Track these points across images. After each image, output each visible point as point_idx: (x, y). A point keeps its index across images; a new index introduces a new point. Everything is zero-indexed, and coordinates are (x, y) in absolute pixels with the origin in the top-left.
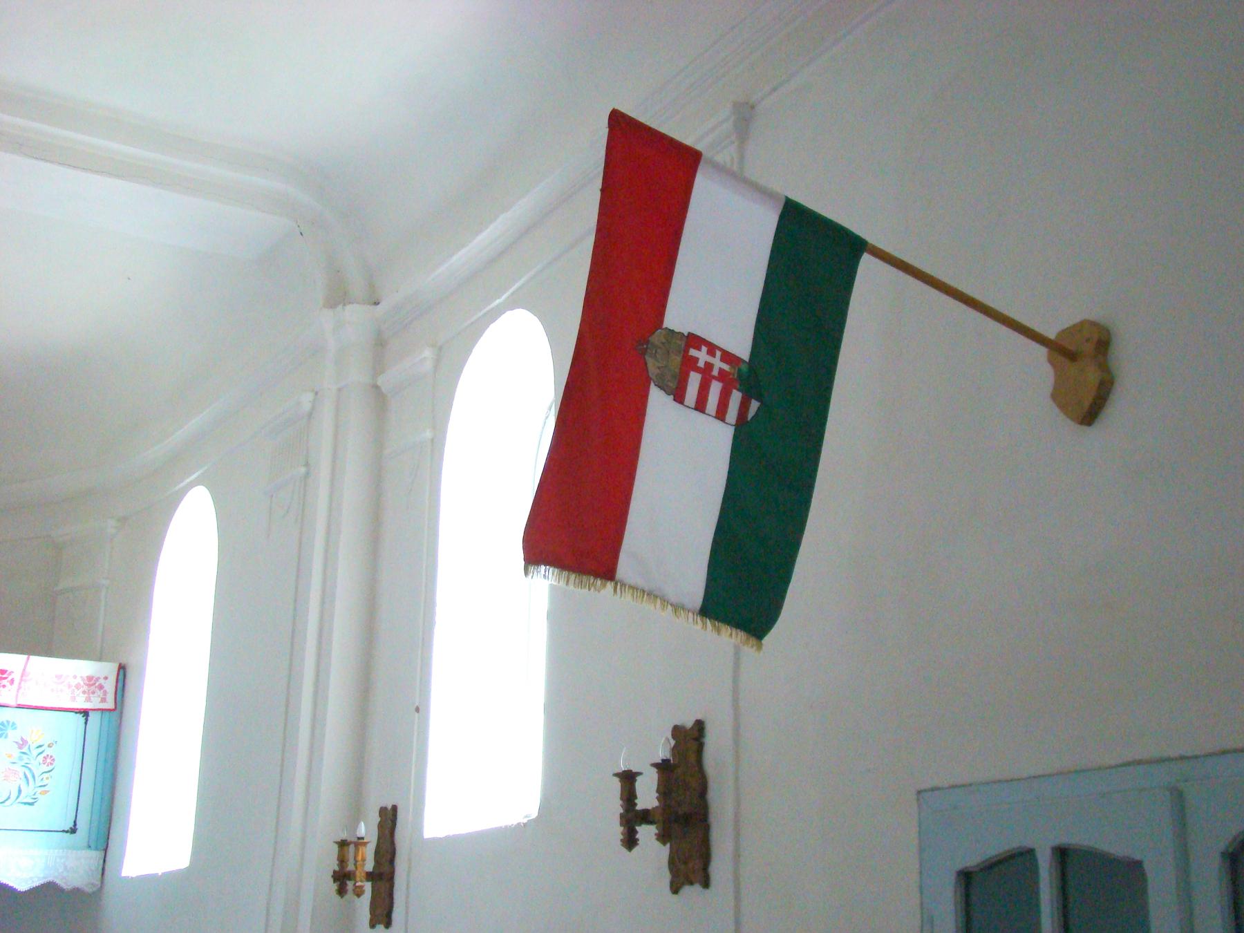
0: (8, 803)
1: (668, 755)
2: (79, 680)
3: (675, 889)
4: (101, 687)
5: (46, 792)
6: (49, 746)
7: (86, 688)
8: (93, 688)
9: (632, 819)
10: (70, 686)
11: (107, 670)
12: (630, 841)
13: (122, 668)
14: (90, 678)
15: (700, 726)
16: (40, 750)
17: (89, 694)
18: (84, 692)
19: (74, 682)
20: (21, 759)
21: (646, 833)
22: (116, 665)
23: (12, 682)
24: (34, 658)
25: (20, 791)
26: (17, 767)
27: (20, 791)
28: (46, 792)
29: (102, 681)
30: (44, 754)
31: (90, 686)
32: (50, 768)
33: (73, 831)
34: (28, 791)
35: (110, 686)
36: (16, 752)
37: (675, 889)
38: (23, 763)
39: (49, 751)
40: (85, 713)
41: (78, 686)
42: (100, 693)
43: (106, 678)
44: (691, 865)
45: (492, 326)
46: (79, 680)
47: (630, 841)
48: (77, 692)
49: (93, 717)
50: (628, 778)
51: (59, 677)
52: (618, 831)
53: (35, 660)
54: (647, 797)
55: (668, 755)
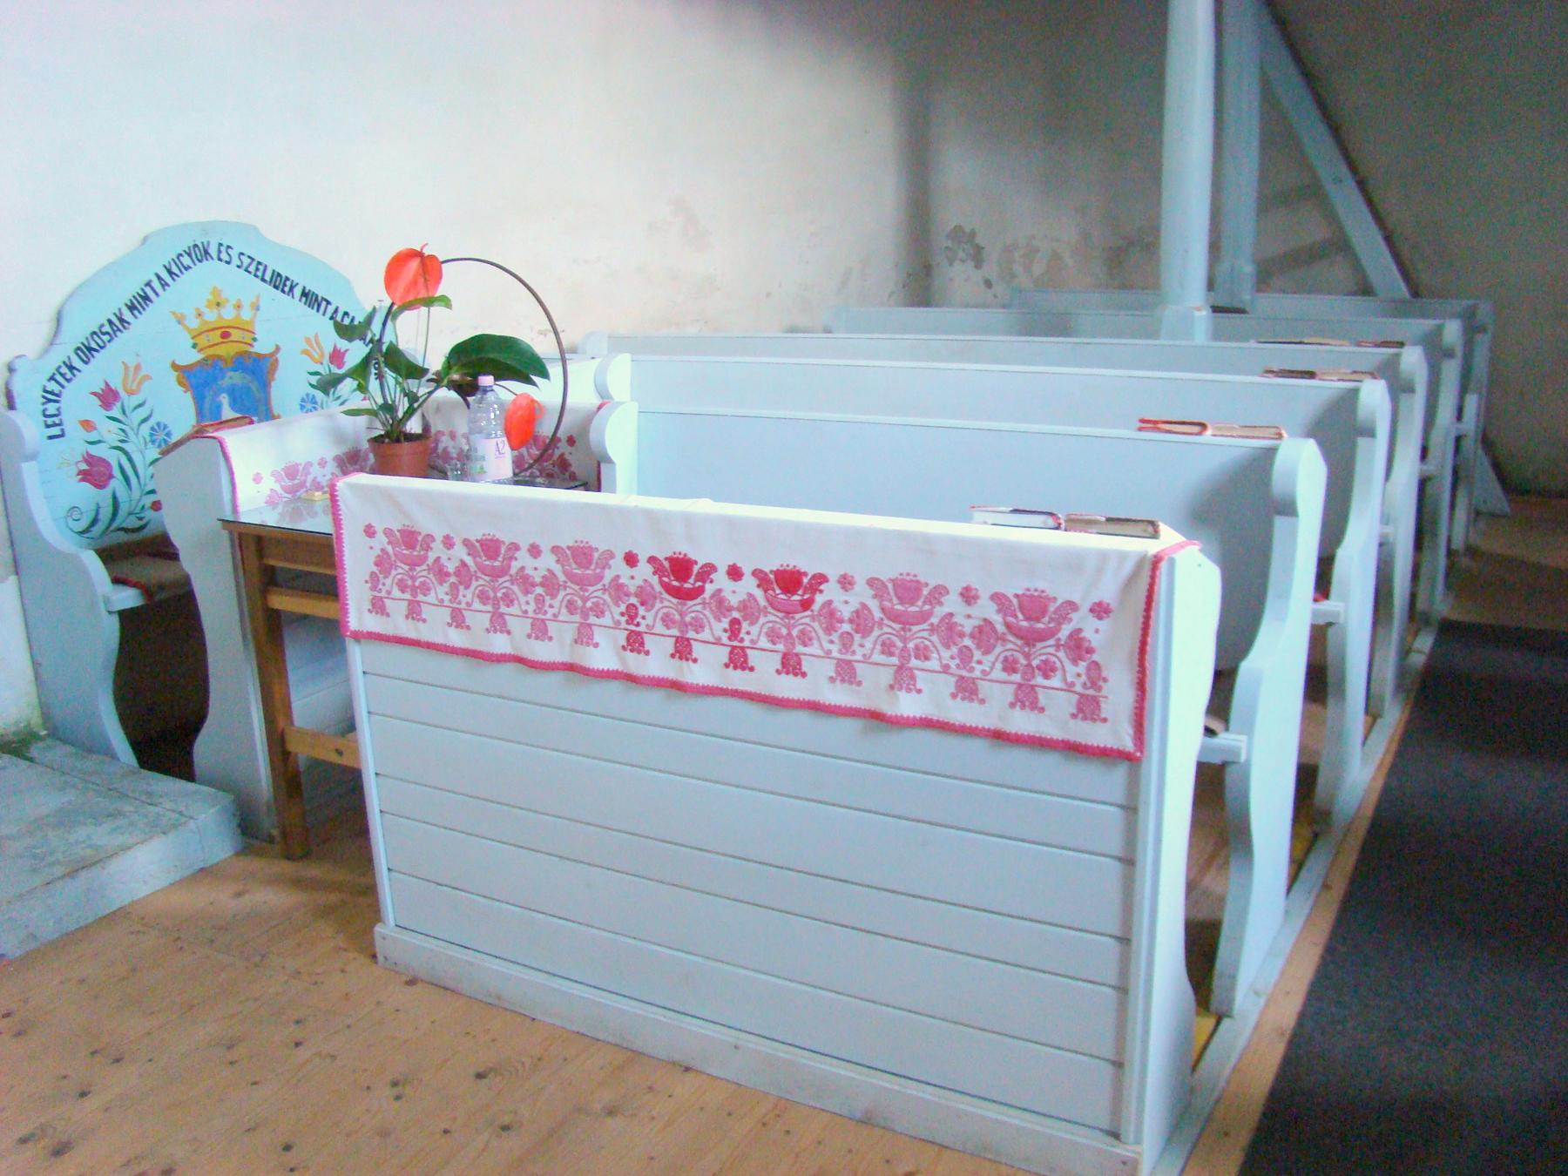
4: (1078, 647)
42: (1075, 671)
46: (986, 609)
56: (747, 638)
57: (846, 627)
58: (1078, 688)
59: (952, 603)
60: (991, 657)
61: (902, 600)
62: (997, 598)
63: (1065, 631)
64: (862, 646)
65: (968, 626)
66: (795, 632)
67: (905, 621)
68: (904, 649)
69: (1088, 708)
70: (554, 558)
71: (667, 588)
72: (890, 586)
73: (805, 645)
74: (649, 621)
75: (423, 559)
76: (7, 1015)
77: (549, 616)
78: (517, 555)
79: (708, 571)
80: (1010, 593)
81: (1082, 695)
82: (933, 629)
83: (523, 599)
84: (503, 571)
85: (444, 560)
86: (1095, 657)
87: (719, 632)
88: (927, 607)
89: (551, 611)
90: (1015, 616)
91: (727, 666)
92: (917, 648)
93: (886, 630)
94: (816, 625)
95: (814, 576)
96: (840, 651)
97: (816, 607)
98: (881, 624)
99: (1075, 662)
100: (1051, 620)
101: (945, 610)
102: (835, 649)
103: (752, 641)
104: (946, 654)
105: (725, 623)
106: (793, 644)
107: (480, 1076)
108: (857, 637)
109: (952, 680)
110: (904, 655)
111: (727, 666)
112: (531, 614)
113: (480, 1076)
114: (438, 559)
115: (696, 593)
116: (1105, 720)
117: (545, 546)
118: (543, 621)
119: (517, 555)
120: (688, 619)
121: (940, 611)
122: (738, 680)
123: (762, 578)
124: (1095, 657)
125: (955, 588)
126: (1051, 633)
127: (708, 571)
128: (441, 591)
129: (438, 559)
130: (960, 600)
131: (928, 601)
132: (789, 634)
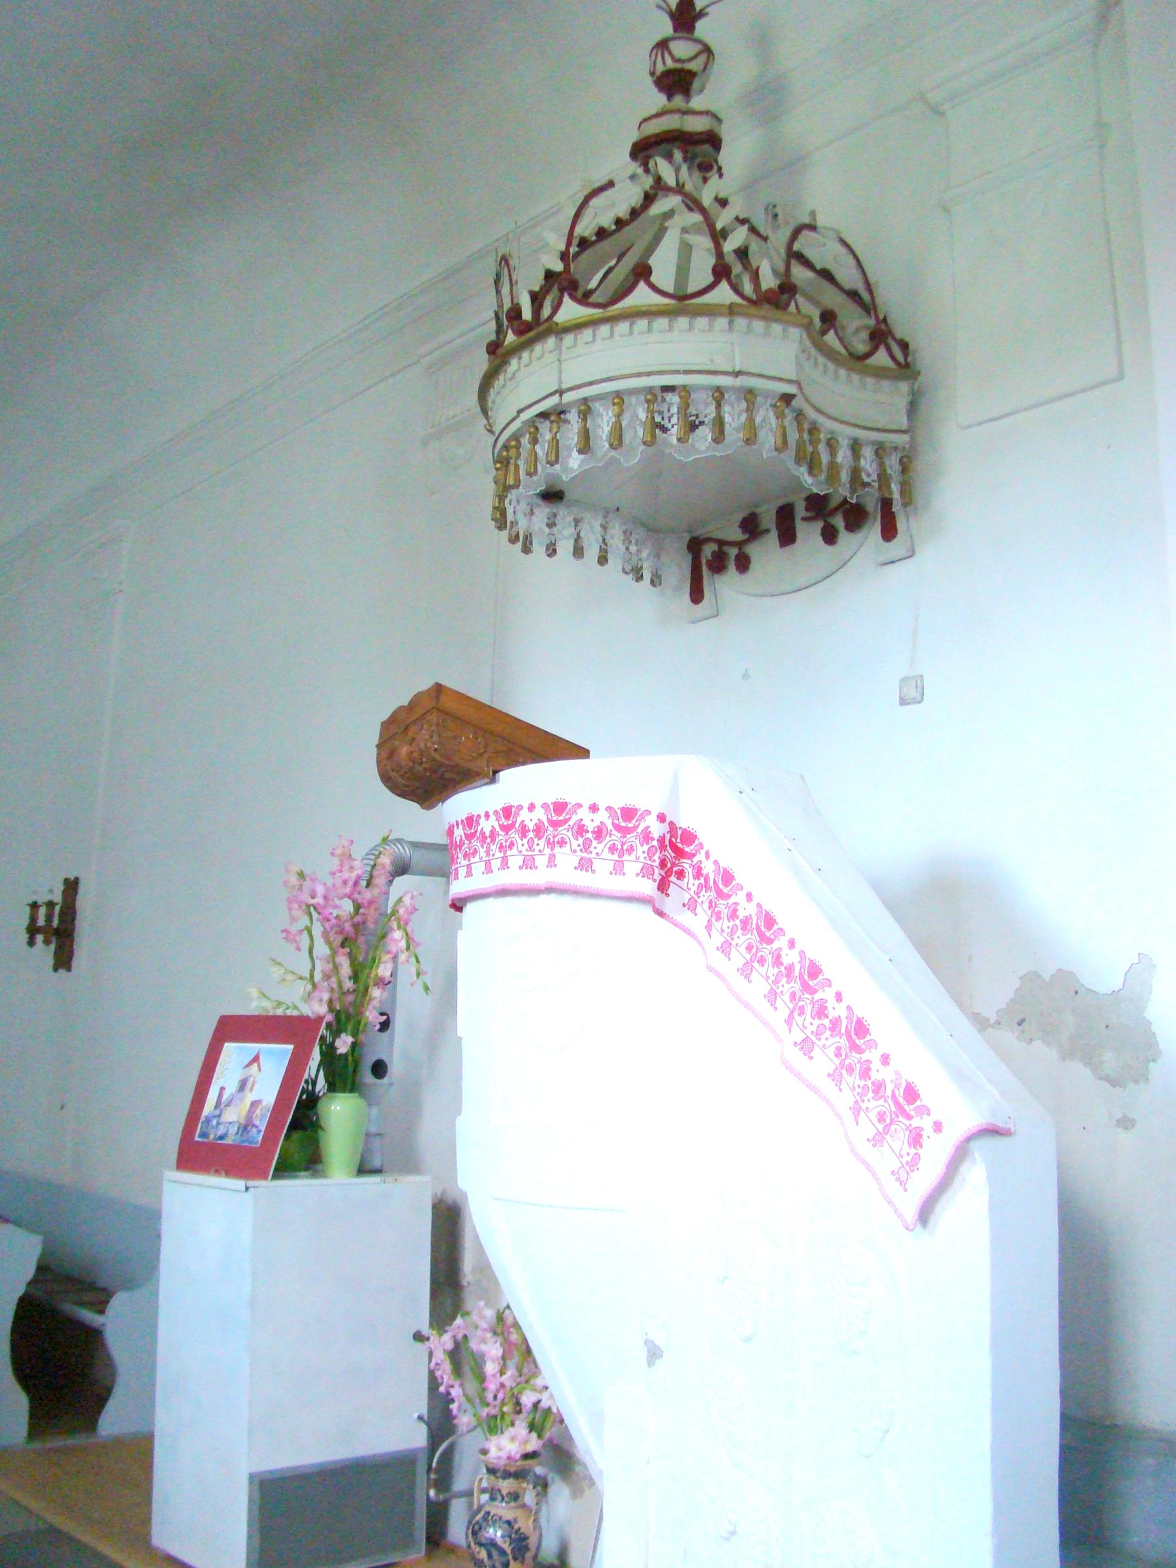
3: (56, 969)
9: (33, 930)
12: (31, 942)
21: (40, 938)
37: (56, 969)
44: (64, 960)
47: (31, 942)
50: (34, 906)
52: (25, 937)
54: (41, 922)
58: (808, 1032)
72: (680, 832)
73: (678, 879)
75: (514, 824)
77: (820, 1043)
78: (826, 989)
79: (924, 1111)
83: (809, 1019)
84: (813, 991)
85: (783, 953)
86: (920, 1151)
92: (850, 1064)
94: (690, 870)
103: (824, 1046)
104: (575, 843)
105: (581, 841)
107: (733, 1533)
108: (828, 1033)
109: (641, 865)
110: (669, 873)
113: (733, 1533)
114: (780, 949)
115: (859, 1050)
118: (813, 1043)
119: (826, 989)
124: (920, 1151)
126: (566, 821)
127: (873, 1044)
128: (727, 924)
129: (780, 949)
130: (745, 896)
132: (671, 868)
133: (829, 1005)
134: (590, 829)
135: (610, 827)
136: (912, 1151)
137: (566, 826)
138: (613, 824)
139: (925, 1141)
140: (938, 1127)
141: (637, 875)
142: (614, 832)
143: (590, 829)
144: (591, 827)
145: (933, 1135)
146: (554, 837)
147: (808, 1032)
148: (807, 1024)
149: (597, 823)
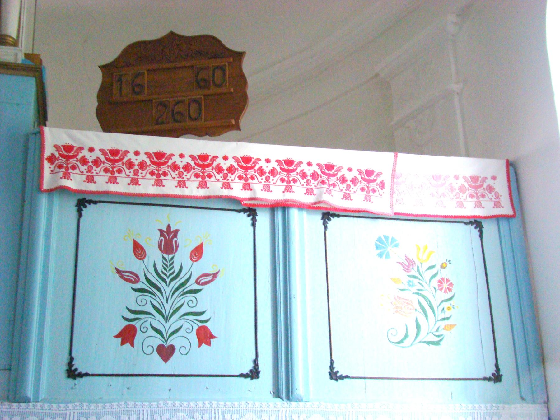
0: (407, 342)
1: (211, 340)
2: (461, 181)
4: (491, 189)
5: (452, 326)
6: (442, 267)
7: (472, 191)
8: (481, 190)
10: (452, 190)
11: (492, 168)
13: (509, 164)
14: (475, 179)
15: (99, 67)
16: (434, 271)
17: (479, 198)
18: (471, 196)
19: (457, 184)
20: (410, 284)
22: (503, 163)
23: (382, 185)
24: (400, 155)
25: (418, 327)
26: (409, 295)
27: (418, 327)
28: (452, 326)
29: (489, 182)
30: (438, 277)
31: (476, 188)
32: (449, 295)
33: (497, 377)
34: (428, 327)
35: (501, 186)
36: (403, 276)
38: (414, 290)
39: (444, 274)
40: (477, 223)
41: (462, 189)
42: (492, 196)
43: (494, 178)
45: (96, 104)
46: (461, 181)
48: (464, 196)
49: (489, 228)
51: (436, 178)
53: (407, 160)
55: (211, 340)
56: (95, 172)
57: (136, 167)
59: (452, 180)
60: (99, 169)
61: (67, 151)
62: (102, 151)
63: (215, 164)
64: (141, 173)
65: (137, 163)
66: (115, 169)
67: (68, 158)
68: (67, 167)
69: (497, 205)
70: (464, 180)
71: (197, 165)
72: (153, 155)
74: (233, 178)
76: (198, 252)
77: (230, 181)
80: (281, 159)
81: (132, 178)
82: (169, 167)
83: (260, 178)
86: (496, 190)
87: (302, 183)
88: (336, 173)
89: (272, 182)
90: (153, 159)
91: (305, 194)
93: (60, 161)
95: (125, 151)
96: (87, 172)
97: (256, 168)
98: (104, 162)
99: (490, 193)
100: (335, 171)
101: (129, 158)
102: (131, 175)
106: (290, 183)
109: (493, 202)
111: (305, 194)
112: (344, 191)
116: (208, 188)
117: (97, 148)
118: (269, 185)
120: (206, 174)
121: (126, 159)
122: (226, 192)
123: (360, 172)
124: (496, 190)
125: (132, 151)
131: (211, 160)
133: (264, 168)
134: (181, 166)
135: (360, 179)
136: (493, 194)
137: (166, 166)
138: (60, 154)
139: (495, 186)
140: (494, 178)
141: (198, 188)
142: (196, 167)
143: (181, 166)
144: (309, 173)
145: (496, 181)
146: (68, 164)
147: (344, 191)
148: (260, 180)
149: (460, 185)
